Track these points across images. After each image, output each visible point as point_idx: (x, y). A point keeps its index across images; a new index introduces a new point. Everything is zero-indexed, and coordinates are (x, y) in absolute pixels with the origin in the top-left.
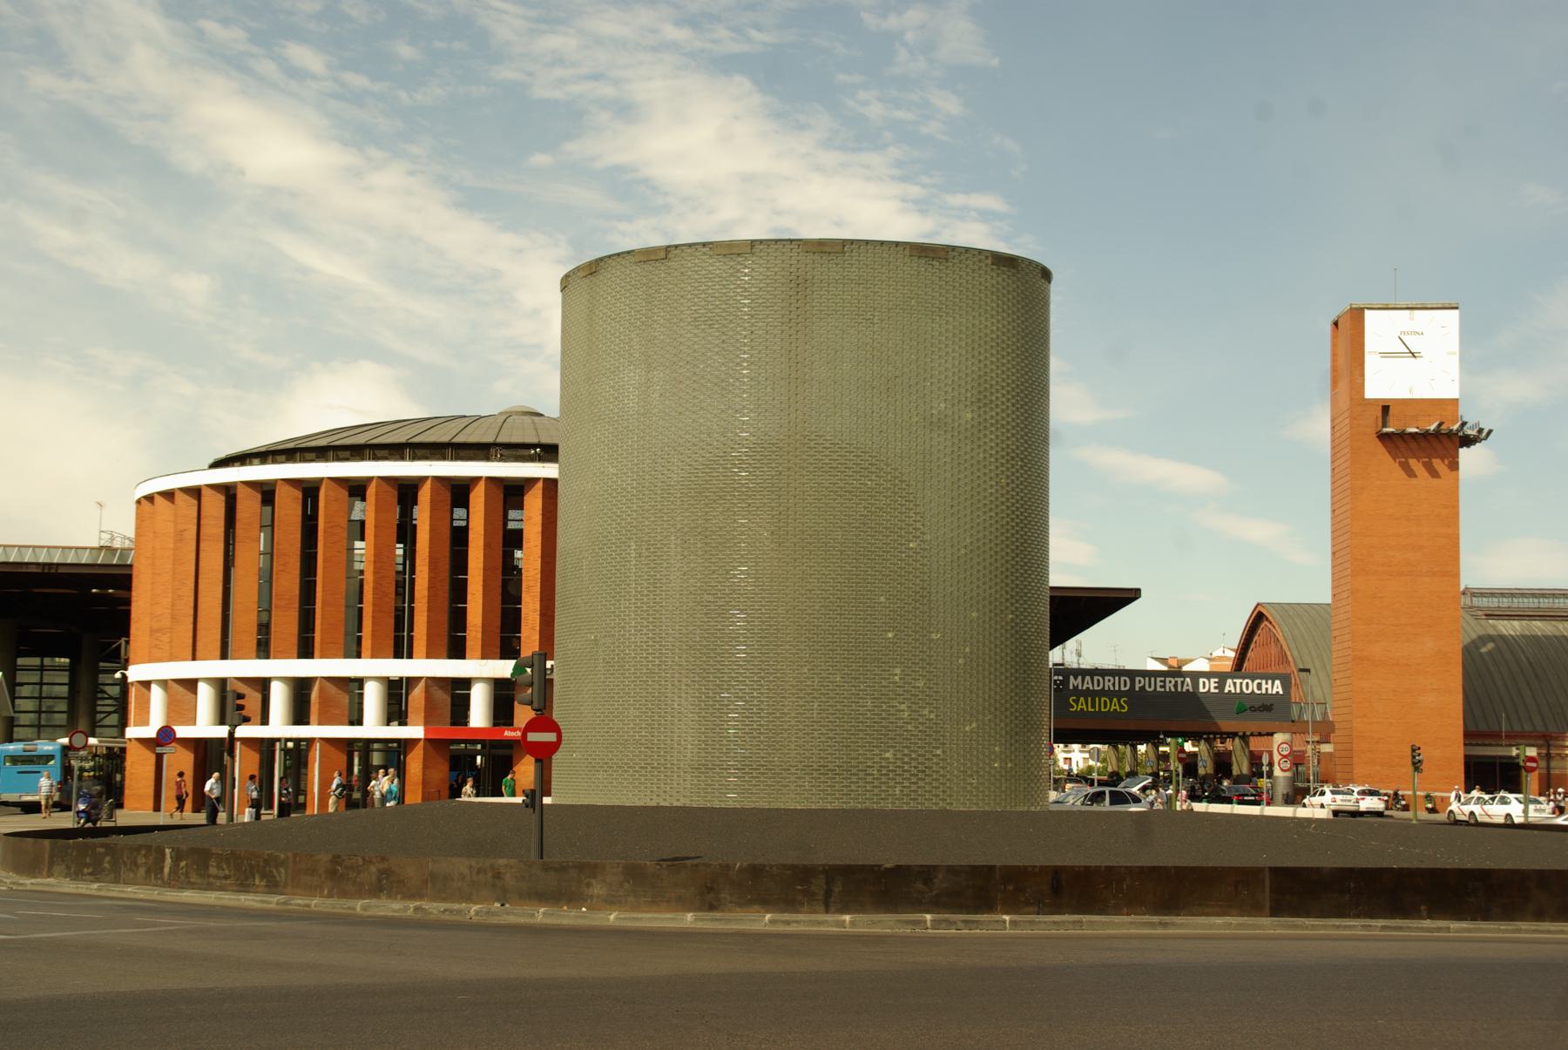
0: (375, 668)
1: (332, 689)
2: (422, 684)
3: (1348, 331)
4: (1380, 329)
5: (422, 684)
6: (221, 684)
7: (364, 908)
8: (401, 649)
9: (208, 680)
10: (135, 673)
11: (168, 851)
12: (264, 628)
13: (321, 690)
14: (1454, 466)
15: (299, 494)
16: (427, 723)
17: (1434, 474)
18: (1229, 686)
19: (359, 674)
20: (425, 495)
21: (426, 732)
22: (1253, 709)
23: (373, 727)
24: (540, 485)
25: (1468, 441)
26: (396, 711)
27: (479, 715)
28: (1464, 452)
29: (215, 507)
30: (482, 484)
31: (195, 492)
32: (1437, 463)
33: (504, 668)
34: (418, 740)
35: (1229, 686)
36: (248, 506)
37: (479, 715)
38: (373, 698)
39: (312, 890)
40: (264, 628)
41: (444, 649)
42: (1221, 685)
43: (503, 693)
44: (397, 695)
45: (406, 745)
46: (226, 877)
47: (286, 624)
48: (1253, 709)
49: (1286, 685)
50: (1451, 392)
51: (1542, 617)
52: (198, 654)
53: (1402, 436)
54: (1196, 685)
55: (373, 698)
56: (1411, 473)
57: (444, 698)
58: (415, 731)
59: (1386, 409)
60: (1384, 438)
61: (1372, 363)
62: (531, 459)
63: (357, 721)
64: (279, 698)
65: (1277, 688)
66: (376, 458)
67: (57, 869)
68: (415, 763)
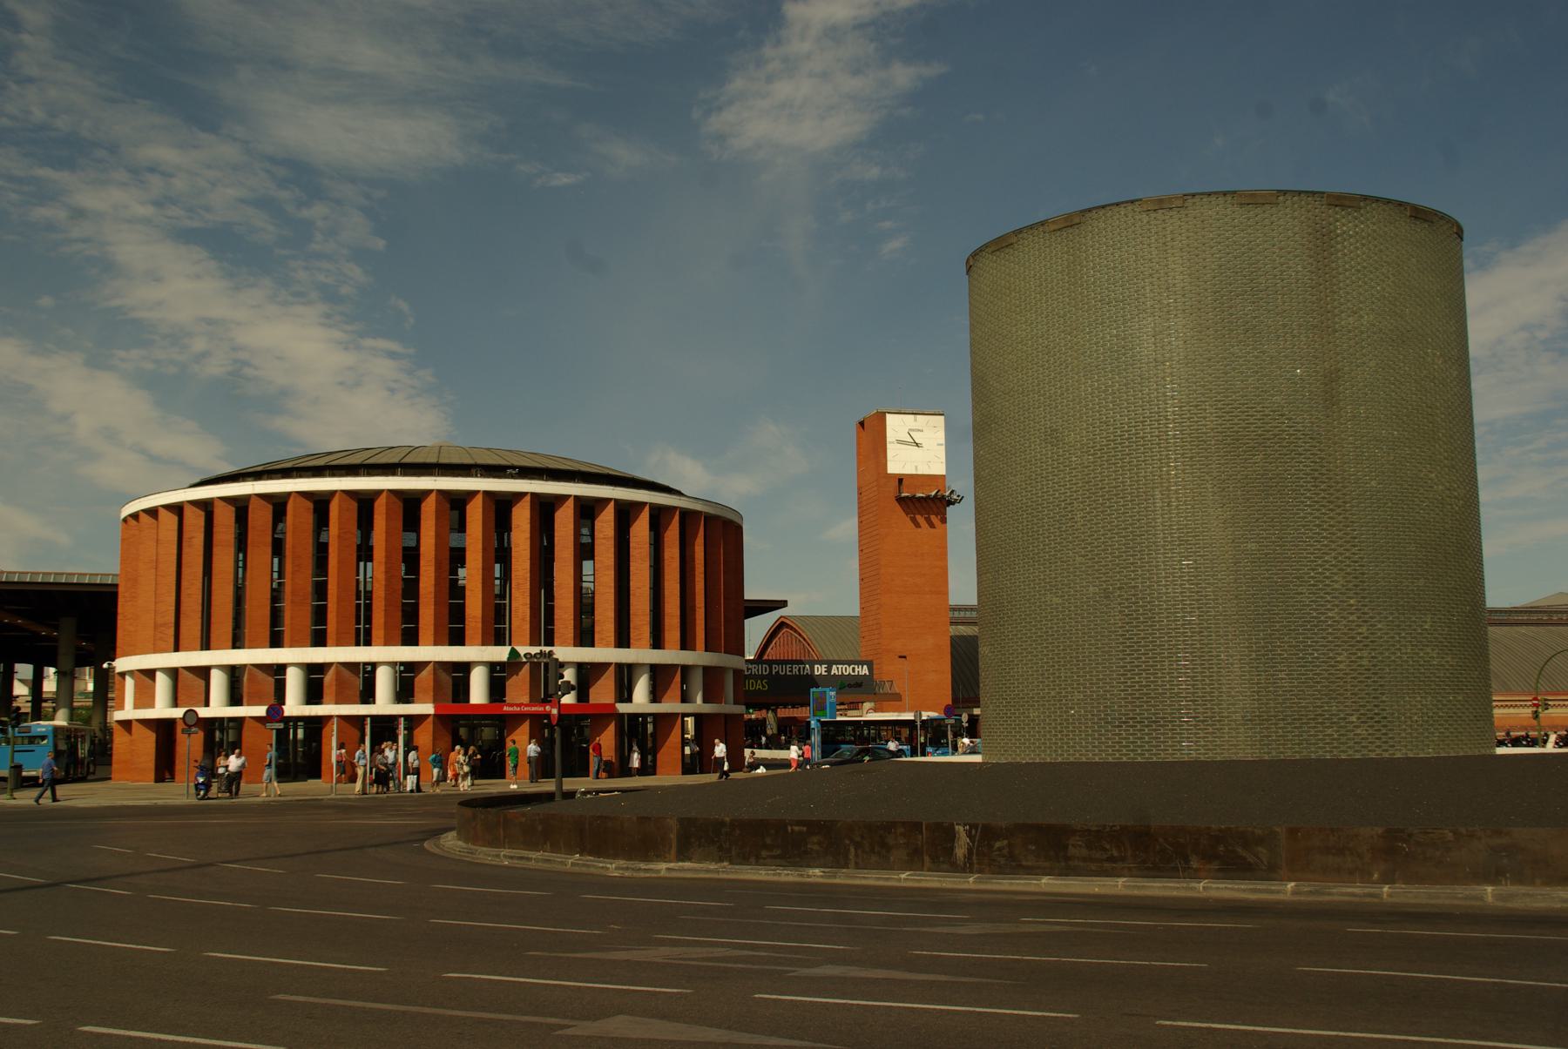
0: (384, 654)
1: (346, 673)
2: (430, 667)
3: (872, 433)
4: (897, 426)
5: (430, 667)
6: (174, 673)
7: (1497, 897)
8: (411, 639)
9: (221, 667)
10: (122, 664)
11: (960, 829)
12: (276, 617)
13: (338, 673)
14: (944, 521)
15: (310, 505)
16: (436, 701)
17: (932, 525)
18: (834, 671)
19: (374, 659)
20: (380, 507)
21: (436, 708)
22: (850, 686)
23: (384, 704)
24: (528, 498)
25: (950, 503)
26: (404, 692)
27: (478, 693)
28: (950, 509)
29: (195, 520)
30: (479, 498)
31: (177, 509)
32: (920, 519)
33: (500, 653)
34: (427, 716)
35: (834, 671)
36: (260, 518)
37: (478, 693)
38: (384, 682)
39: (1362, 874)
40: (276, 617)
41: (446, 638)
42: (829, 670)
43: (499, 676)
44: (406, 680)
45: (413, 721)
46: (1123, 859)
47: (296, 614)
48: (850, 686)
49: (870, 669)
50: (939, 468)
51: (963, 623)
52: (182, 642)
53: (913, 499)
54: (812, 669)
55: (384, 682)
56: (917, 525)
57: (446, 679)
58: (426, 708)
59: (901, 481)
60: (900, 500)
61: (893, 450)
62: (512, 477)
63: (152, 705)
64: (218, 682)
65: (865, 671)
66: (369, 475)
67: (1538, 881)
68: (424, 736)
